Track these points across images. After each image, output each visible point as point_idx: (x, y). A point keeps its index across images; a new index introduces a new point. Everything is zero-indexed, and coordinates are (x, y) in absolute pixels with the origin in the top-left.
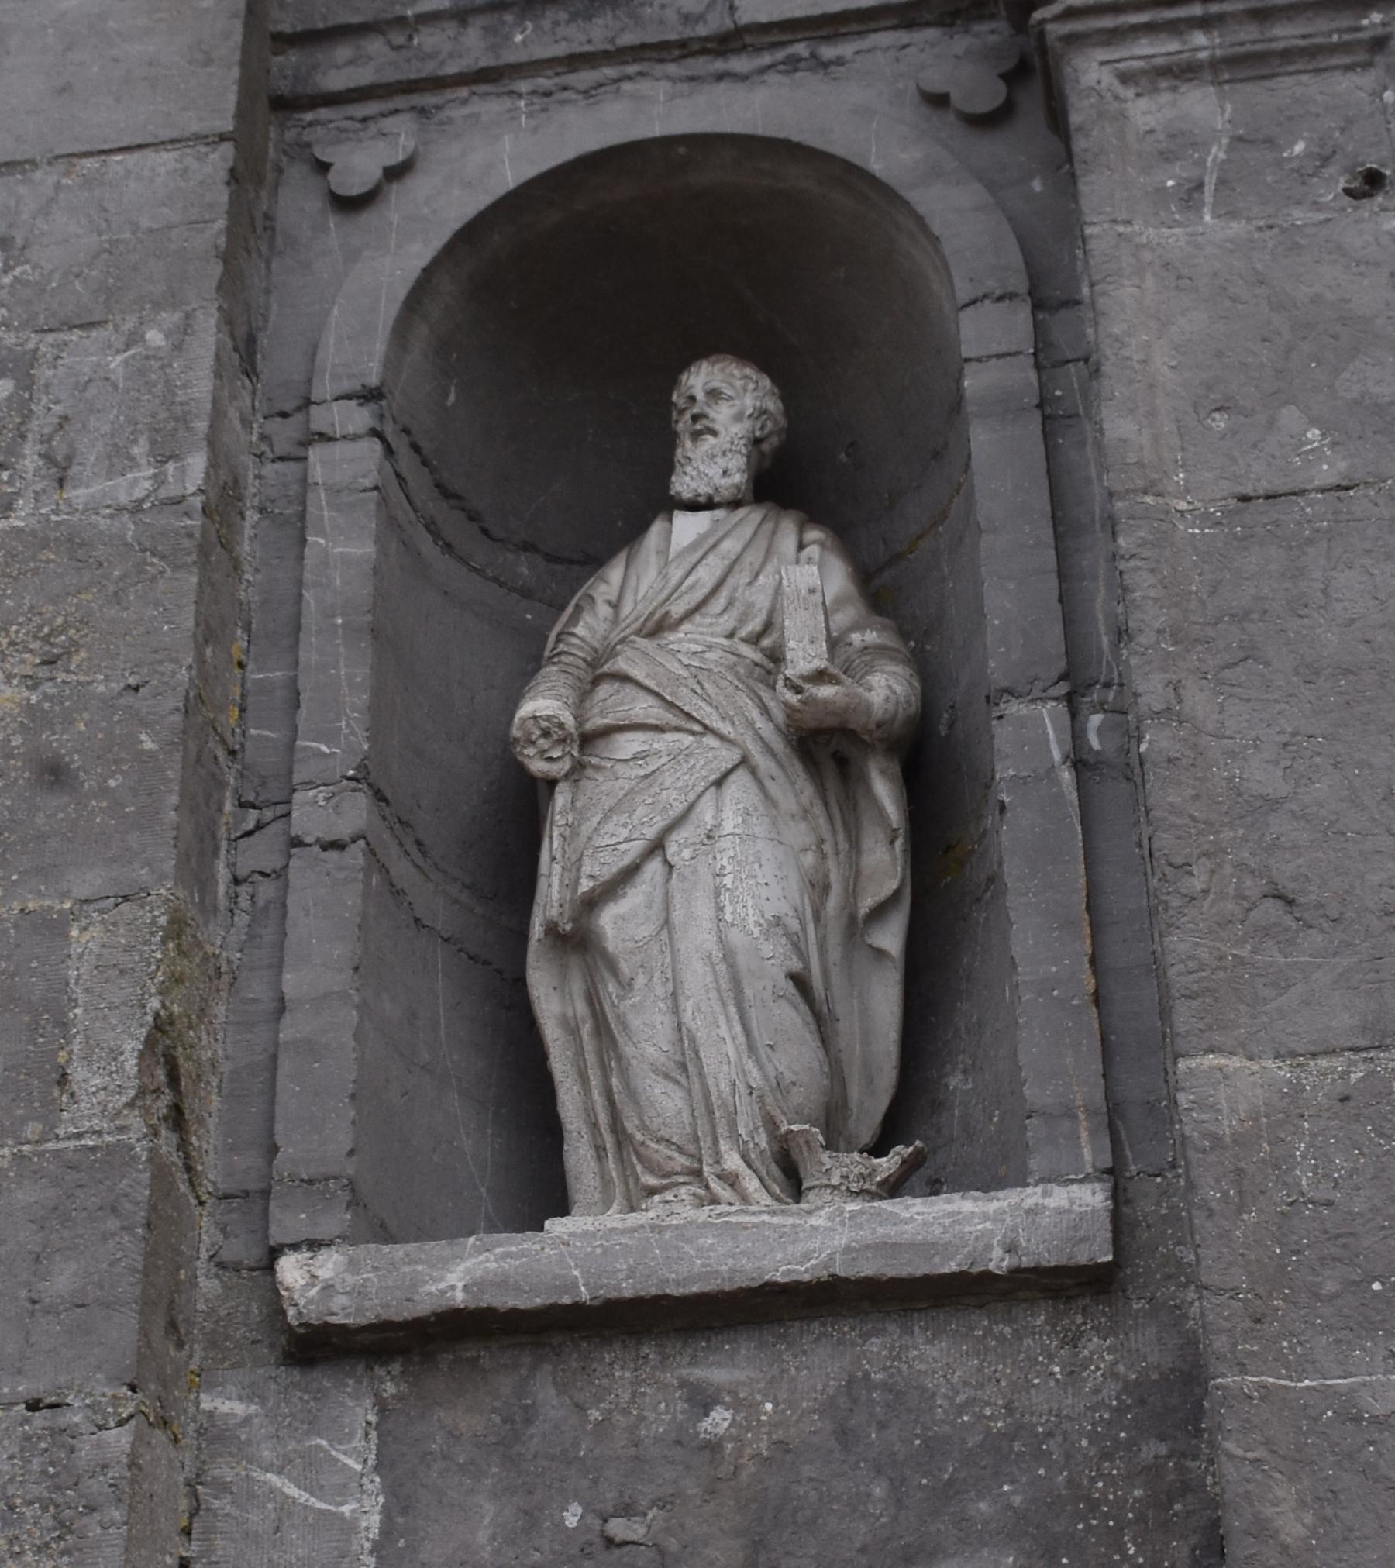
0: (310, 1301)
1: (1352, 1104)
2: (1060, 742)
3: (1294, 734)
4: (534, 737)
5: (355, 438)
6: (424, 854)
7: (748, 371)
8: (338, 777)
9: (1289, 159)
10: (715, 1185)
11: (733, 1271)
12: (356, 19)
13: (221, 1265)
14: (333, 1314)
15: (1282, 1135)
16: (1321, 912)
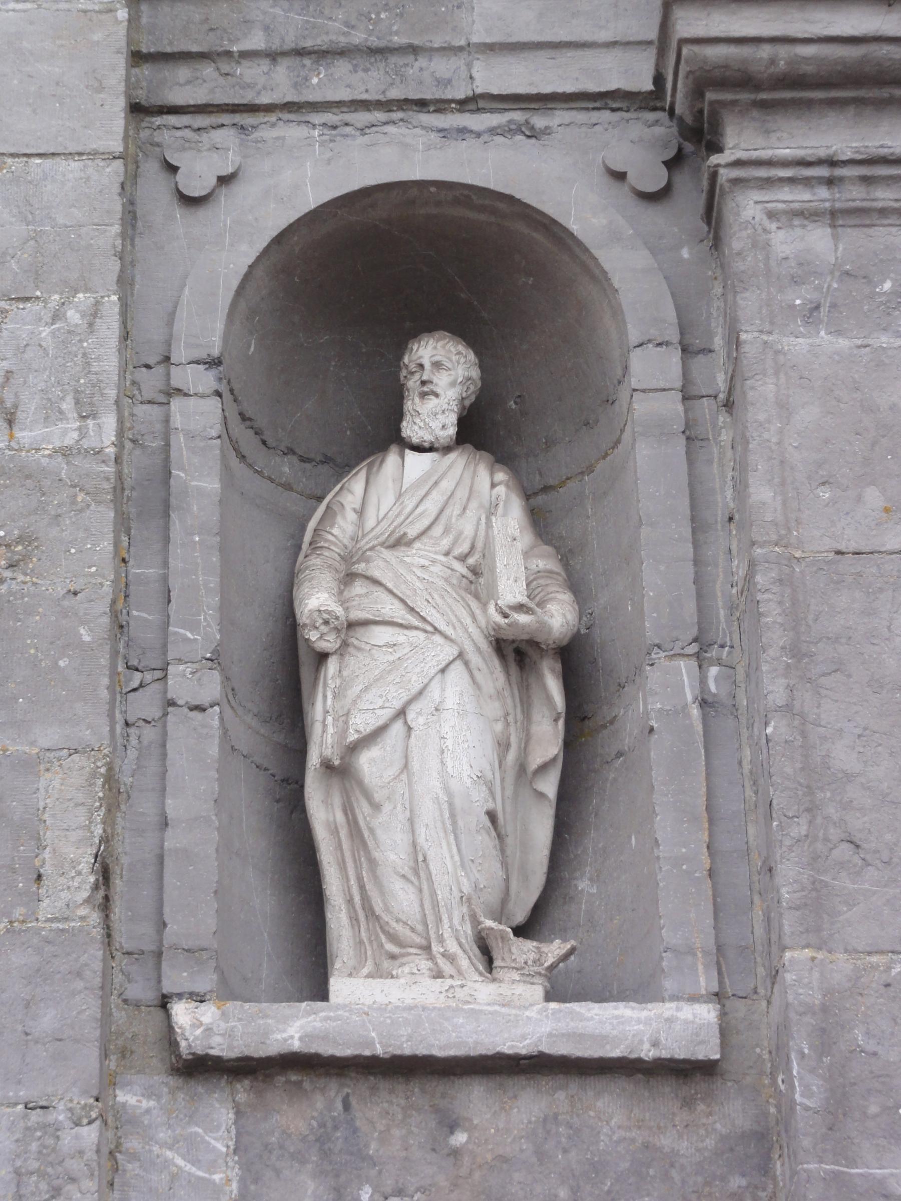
0: (196, 1038)
1: (892, 989)
2: (692, 687)
3: (865, 729)
4: (317, 625)
5: (203, 396)
6: (234, 695)
7: (461, 348)
8: (199, 658)
9: (881, 294)
10: (441, 961)
11: (476, 1043)
12: (195, 48)
13: (125, 1001)
14: (212, 1048)
15: (848, 1006)
16: (878, 855)
